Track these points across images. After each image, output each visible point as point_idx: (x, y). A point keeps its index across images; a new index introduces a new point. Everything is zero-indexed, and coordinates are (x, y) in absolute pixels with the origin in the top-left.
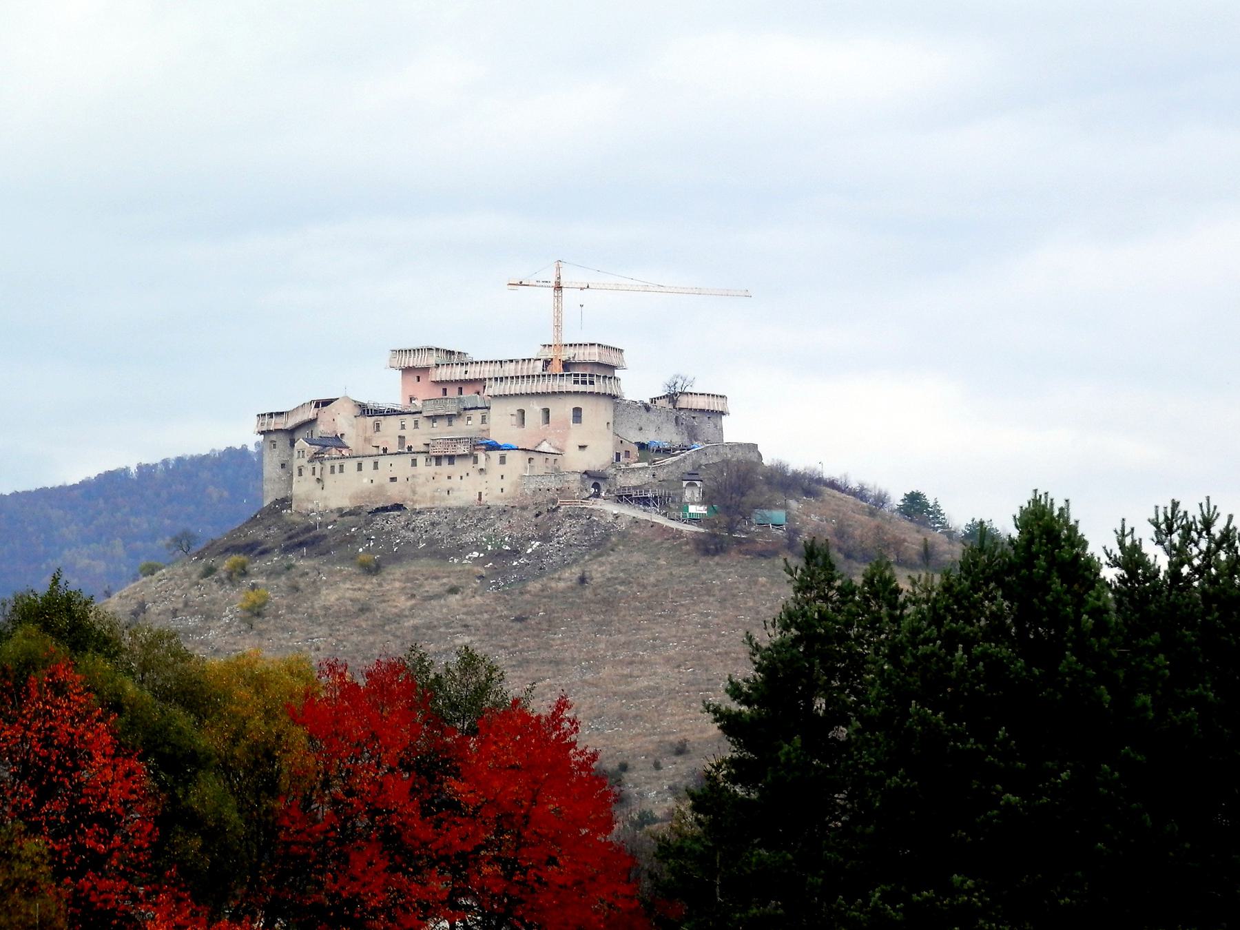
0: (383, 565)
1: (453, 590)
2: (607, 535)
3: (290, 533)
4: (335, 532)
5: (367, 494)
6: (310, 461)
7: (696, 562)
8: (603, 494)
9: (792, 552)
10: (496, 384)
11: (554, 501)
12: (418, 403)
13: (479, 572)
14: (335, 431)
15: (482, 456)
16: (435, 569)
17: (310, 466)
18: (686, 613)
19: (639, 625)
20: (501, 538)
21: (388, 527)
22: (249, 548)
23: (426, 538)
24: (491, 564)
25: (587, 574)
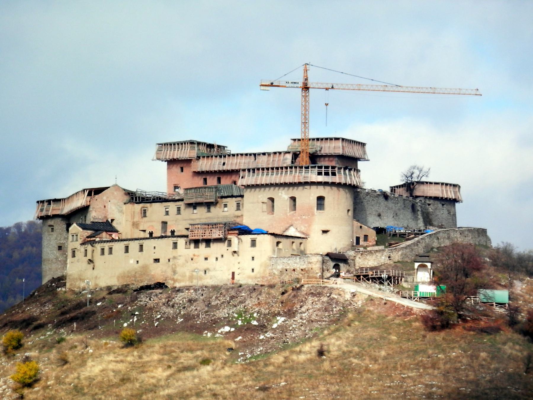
0: (144, 338)
1: (205, 362)
2: (345, 312)
3: (63, 310)
4: (102, 308)
5: (133, 273)
6: (83, 244)
7: (424, 336)
8: (342, 274)
9: (512, 328)
10: (249, 176)
11: (298, 280)
12: (181, 191)
13: (229, 345)
14: (106, 217)
15: (234, 239)
16: (191, 342)
17: (82, 249)
18: (412, 384)
19: (369, 395)
20: (251, 314)
21: (151, 304)
22: (25, 324)
23: (184, 314)
24: (240, 338)
25: (325, 348)
